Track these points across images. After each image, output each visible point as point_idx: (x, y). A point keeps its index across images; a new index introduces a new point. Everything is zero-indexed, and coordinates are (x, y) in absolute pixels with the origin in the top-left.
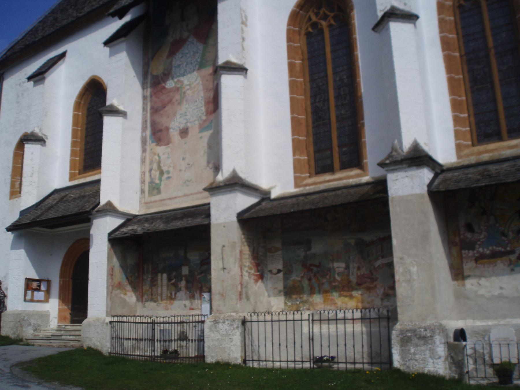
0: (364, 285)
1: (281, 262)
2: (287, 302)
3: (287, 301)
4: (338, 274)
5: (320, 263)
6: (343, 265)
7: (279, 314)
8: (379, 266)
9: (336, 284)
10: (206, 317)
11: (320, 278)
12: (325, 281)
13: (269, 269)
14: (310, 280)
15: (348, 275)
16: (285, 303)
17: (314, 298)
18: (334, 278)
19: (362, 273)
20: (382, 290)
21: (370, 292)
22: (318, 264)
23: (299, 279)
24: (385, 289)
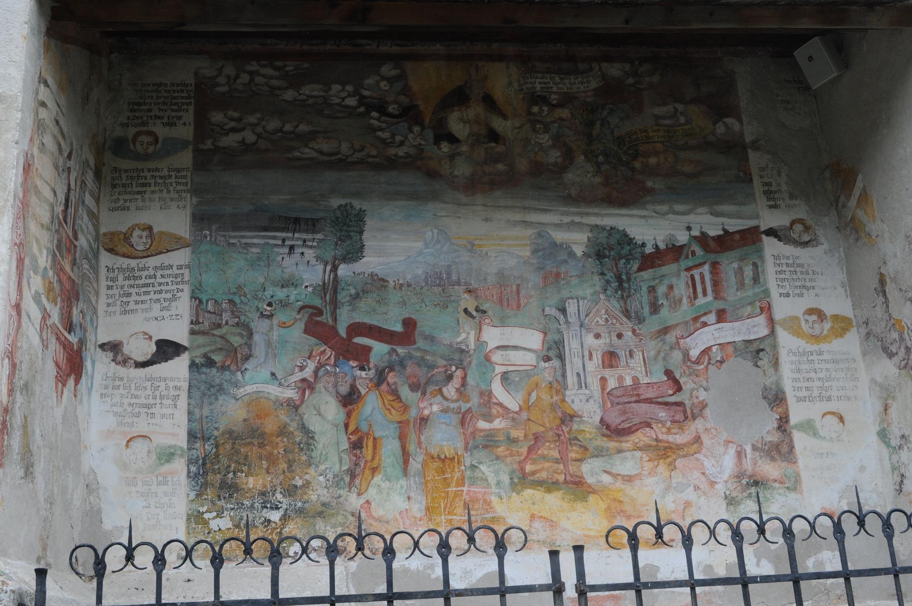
0: (642, 437)
1: (184, 306)
2: (208, 511)
3: (204, 509)
4: (505, 377)
5: (410, 324)
6: (534, 339)
7: (838, 531)
8: (706, 351)
9: (498, 424)
10: (324, 485)
11: (405, 392)
12: (435, 408)
13: (103, 338)
14: (350, 399)
15: (559, 386)
16: (196, 518)
17: (372, 492)
18: (487, 396)
19: (628, 382)
20: (729, 461)
21: (672, 467)
22: (398, 328)
23: (291, 394)
24: (740, 454)
